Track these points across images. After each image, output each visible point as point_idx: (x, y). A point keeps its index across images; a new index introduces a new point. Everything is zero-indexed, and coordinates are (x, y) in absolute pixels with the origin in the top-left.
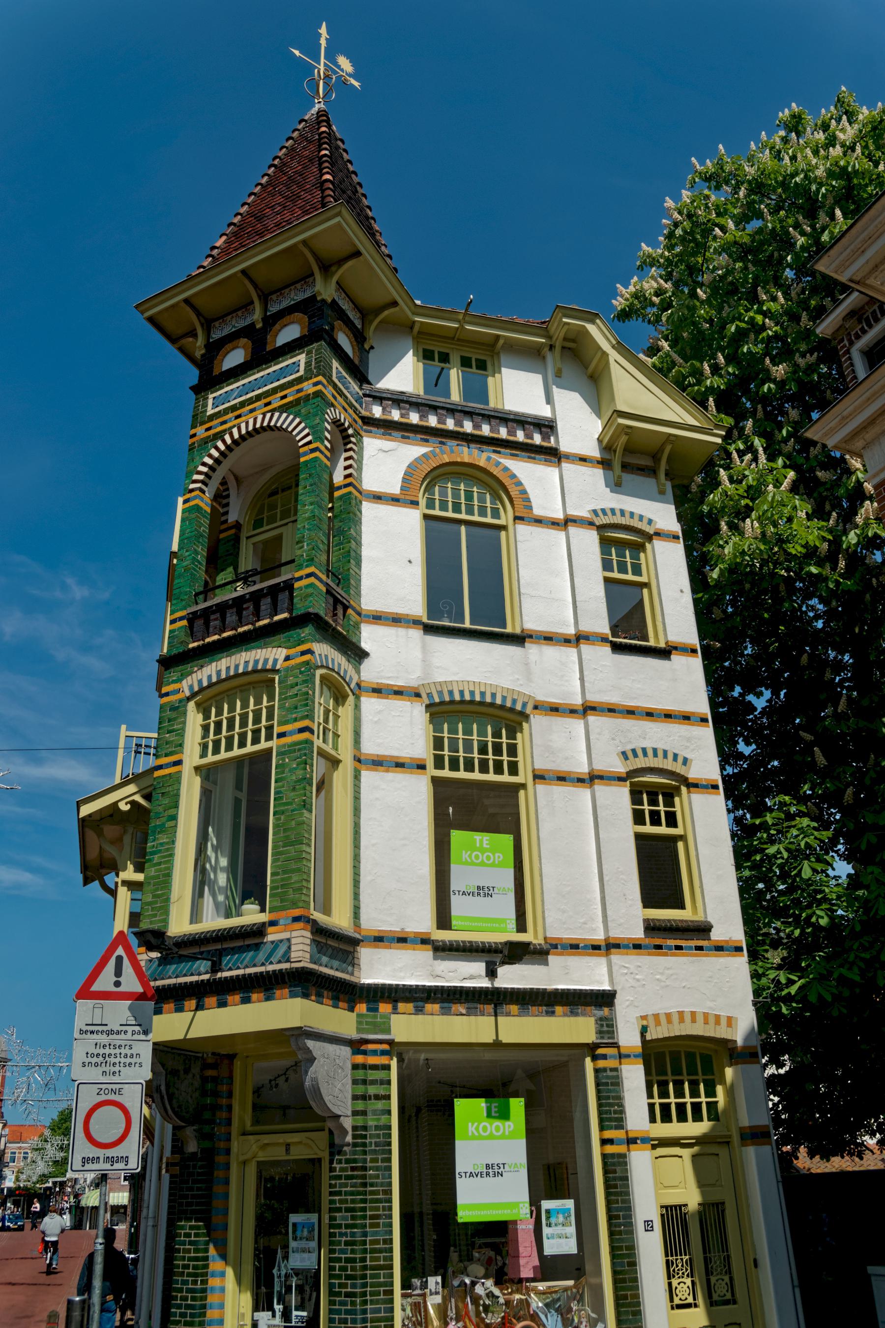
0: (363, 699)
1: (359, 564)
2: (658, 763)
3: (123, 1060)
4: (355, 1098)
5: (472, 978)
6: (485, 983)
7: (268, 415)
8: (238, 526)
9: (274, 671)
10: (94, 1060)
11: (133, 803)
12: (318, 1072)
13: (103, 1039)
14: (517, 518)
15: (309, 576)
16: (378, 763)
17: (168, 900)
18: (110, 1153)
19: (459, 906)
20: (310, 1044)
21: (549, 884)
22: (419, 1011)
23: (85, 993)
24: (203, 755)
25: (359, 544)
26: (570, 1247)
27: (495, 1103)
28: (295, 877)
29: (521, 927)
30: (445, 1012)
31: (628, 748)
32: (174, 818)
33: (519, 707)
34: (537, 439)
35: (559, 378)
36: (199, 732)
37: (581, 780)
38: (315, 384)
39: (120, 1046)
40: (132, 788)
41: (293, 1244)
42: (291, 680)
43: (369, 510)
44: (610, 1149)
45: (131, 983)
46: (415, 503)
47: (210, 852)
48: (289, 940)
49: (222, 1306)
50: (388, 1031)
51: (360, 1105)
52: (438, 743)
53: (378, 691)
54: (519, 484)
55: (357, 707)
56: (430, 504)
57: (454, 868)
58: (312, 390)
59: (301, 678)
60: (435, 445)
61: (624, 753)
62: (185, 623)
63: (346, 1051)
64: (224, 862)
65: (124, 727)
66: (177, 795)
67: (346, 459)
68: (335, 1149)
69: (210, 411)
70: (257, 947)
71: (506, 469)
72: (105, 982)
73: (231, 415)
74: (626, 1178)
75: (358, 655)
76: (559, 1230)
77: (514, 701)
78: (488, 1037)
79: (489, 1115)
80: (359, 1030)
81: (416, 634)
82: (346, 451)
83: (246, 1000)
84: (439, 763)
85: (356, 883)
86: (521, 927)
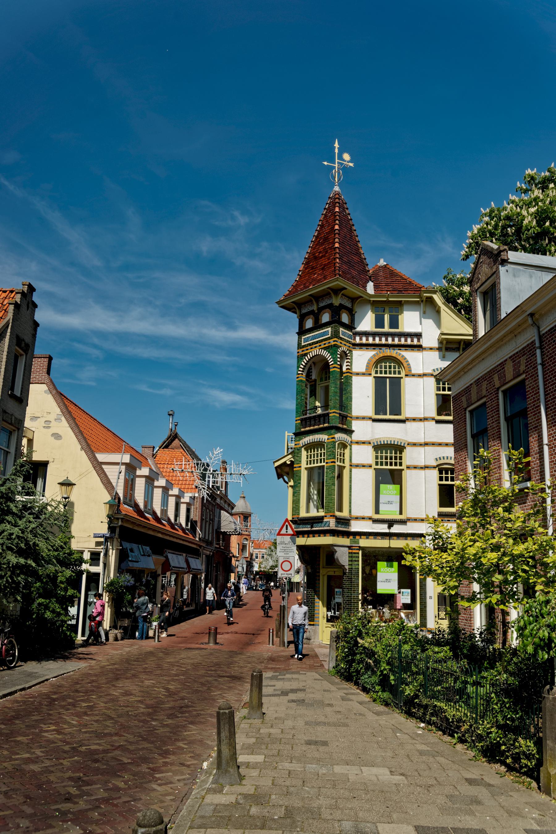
0: (353, 446)
1: (351, 401)
2: (446, 461)
4: (349, 561)
5: (383, 529)
6: (387, 531)
8: (315, 380)
9: (324, 442)
11: (291, 461)
12: (337, 555)
13: (284, 546)
14: (406, 375)
16: (357, 466)
17: (299, 507)
18: (288, 573)
19: (382, 507)
20: (335, 548)
21: (408, 501)
22: (367, 538)
23: (279, 534)
24: (307, 464)
25: (351, 394)
26: (408, 601)
27: (389, 563)
28: (331, 505)
29: (401, 513)
30: (375, 539)
31: (438, 457)
32: (300, 483)
33: (402, 445)
34: (415, 342)
35: (424, 315)
36: (306, 457)
37: (422, 468)
38: (334, 341)
40: (290, 456)
41: (336, 596)
42: (329, 446)
43: (355, 379)
45: (290, 531)
46: (370, 374)
47: (311, 490)
49: (319, 610)
50: (358, 544)
51: (350, 563)
52: (377, 458)
53: (357, 443)
54: (407, 361)
55: (351, 449)
56: (376, 372)
57: (381, 496)
58: (333, 343)
59: (332, 446)
61: (436, 459)
62: (299, 421)
63: (347, 549)
64: (316, 492)
65: (286, 432)
66: (300, 477)
67: (347, 366)
68: (345, 573)
69: (303, 344)
70: (322, 522)
71: (403, 356)
72: (284, 531)
73: (309, 347)
74: (426, 585)
76: (406, 597)
77: (401, 443)
78: (387, 546)
79: (387, 566)
80: (351, 543)
81: (370, 422)
82: (347, 359)
83: (319, 536)
84: (377, 464)
85: (350, 503)
86: (401, 513)
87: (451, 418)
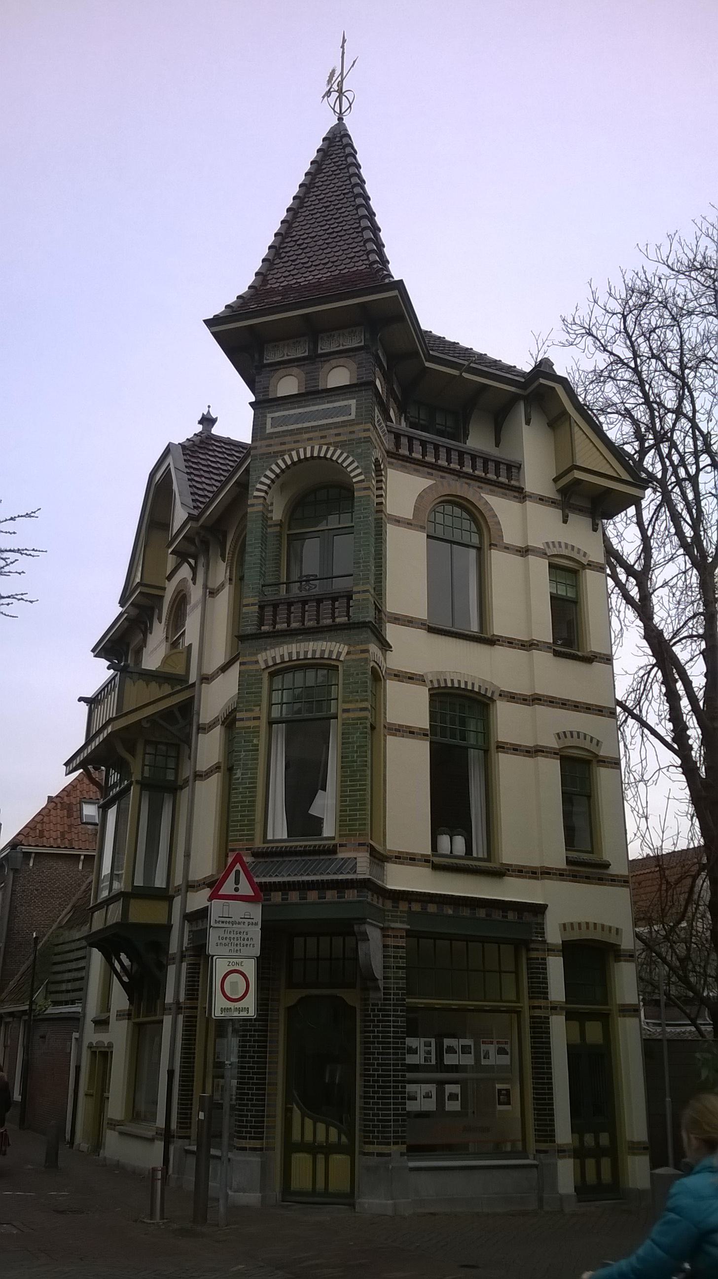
3: (242, 942)
7: (325, 448)
10: (224, 941)
15: (364, 591)
33: (489, 695)
39: (240, 933)
43: (391, 530)
44: (537, 1013)
45: (246, 889)
48: (356, 858)
60: (437, 479)
61: (558, 734)
75: (385, 646)
81: (423, 633)
87: (284, 716)
